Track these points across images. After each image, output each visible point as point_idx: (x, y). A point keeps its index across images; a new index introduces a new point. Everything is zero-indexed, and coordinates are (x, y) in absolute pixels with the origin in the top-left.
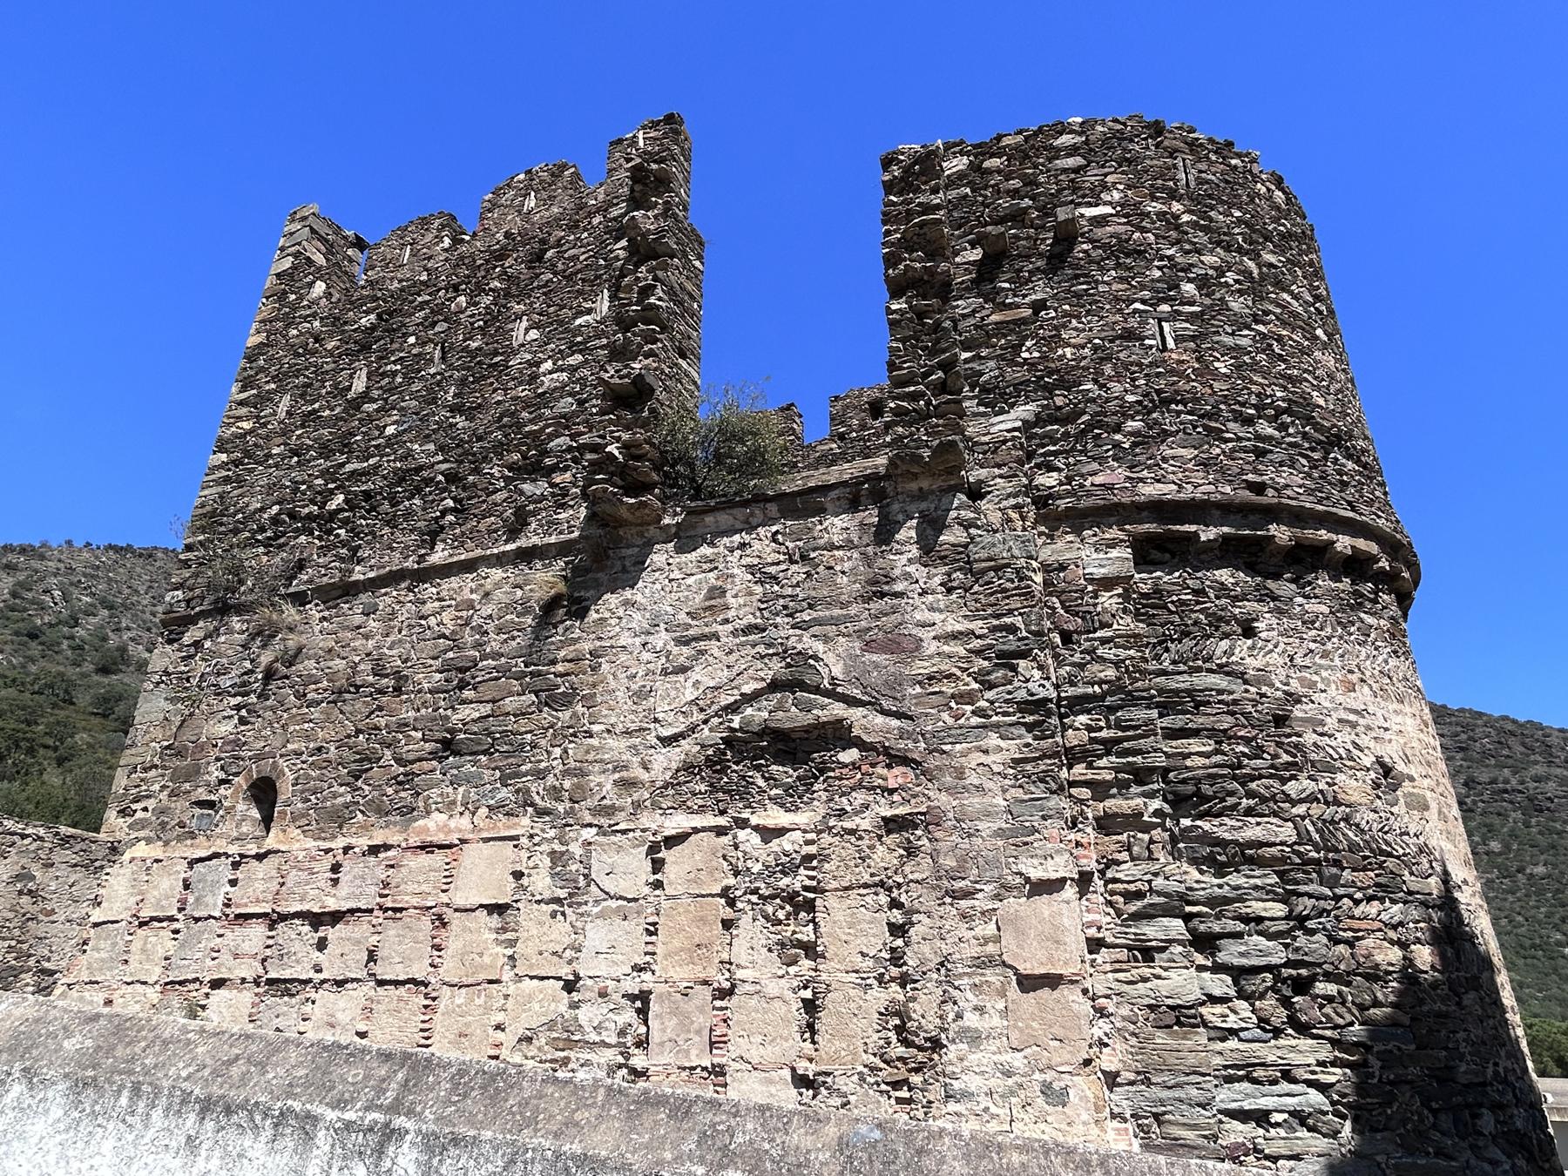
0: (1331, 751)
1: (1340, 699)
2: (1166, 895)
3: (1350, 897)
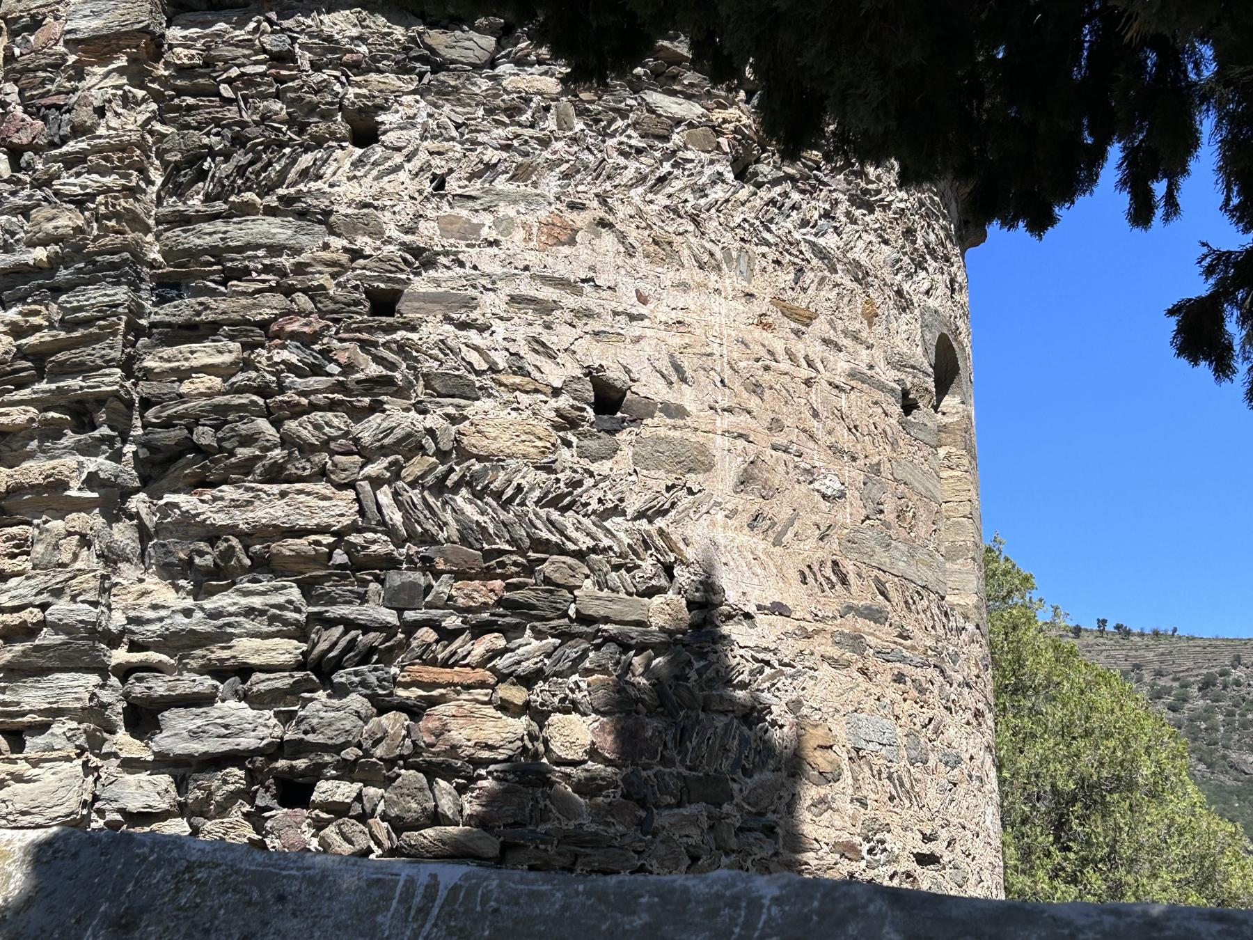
0: (474, 357)
1: (531, 258)
2: (68, 629)
3: (434, 624)
